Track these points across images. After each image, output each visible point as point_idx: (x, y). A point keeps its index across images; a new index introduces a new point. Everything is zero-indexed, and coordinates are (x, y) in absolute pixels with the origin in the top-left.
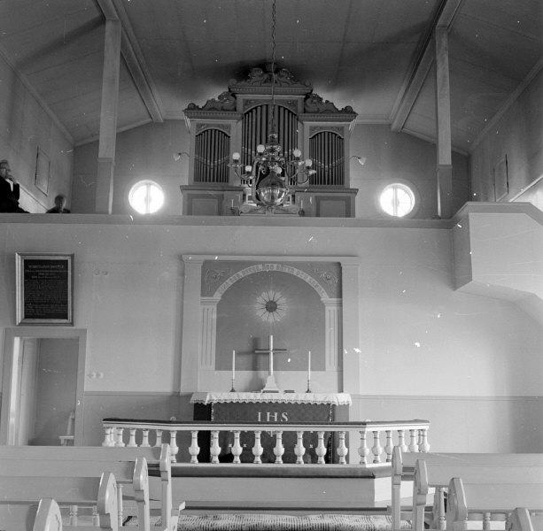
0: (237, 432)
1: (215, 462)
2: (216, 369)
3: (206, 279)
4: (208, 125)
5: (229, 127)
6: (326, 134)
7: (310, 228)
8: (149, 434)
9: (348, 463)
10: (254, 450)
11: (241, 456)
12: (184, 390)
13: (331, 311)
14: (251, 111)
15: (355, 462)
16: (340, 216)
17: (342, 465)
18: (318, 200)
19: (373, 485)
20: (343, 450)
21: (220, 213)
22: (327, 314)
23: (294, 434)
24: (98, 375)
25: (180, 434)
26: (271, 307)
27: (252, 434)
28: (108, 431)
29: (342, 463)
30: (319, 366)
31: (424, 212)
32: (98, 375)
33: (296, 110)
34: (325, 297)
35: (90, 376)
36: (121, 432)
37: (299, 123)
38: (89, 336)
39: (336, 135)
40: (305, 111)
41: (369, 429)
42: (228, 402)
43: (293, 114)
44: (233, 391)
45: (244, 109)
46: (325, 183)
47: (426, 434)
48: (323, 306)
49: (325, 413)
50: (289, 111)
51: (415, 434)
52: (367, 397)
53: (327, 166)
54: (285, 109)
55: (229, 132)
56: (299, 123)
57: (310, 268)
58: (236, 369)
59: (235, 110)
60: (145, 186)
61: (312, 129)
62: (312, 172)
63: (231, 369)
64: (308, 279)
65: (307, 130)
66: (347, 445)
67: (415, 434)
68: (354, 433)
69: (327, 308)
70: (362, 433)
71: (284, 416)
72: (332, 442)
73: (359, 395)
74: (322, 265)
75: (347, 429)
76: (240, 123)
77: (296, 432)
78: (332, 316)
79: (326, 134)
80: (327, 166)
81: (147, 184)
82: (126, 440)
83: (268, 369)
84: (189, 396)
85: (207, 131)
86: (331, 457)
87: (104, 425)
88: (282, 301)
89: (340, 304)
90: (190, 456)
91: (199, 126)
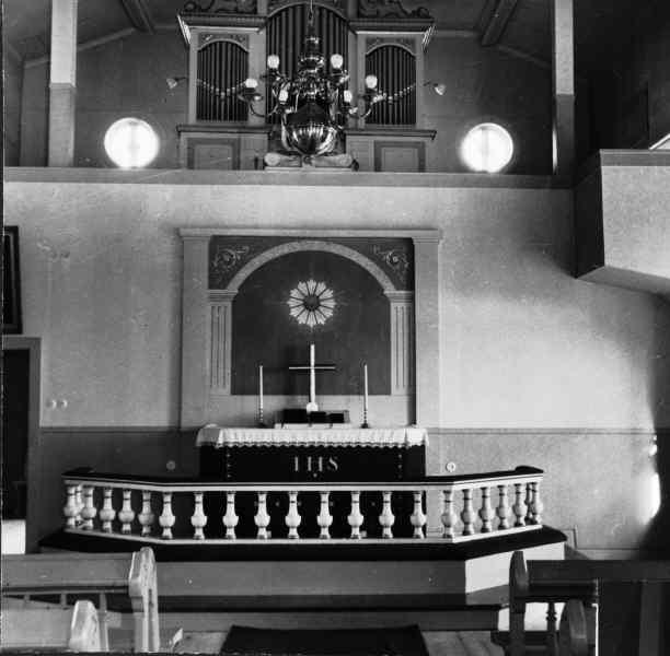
0: (109, 488)
1: (230, 538)
2: (234, 392)
3: (216, 265)
4: (215, 36)
5: (246, 38)
6: (224, 45)
7: (215, 187)
8: (172, 498)
9: (425, 536)
10: (382, 520)
11: (204, 528)
12: (188, 422)
13: (398, 310)
14: (279, 14)
15: (434, 537)
16: (36, 165)
17: (420, 538)
18: (378, 146)
19: (464, 565)
20: (419, 517)
21: (236, 166)
22: (393, 312)
23: (378, 496)
24: (60, 404)
25: (302, 496)
26: (311, 304)
27: (378, 496)
28: (72, 491)
29: (418, 537)
30: (382, 387)
31: (528, 165)
32: (60, 404)
33: (345, 13)
34: (389, 290)
35: (49, 404)
36: (91, 492)
37: (350, 34)
38: (44, 347)
39: (404, 50)
40: (359, 15)
41: (458, 487)
42: (316, 445)
43: (341, 19)
44: (365, 426)
45: (269, 11)
46: (220, 118)
47: (537, 488)
48: (386, 302)
49: (405, 463)
50: (336, 15)
51: (523, 489)
52: (447, 432)
53: (223, 94)
54: (329, 11)
55: (248, 48)
56: (350, 34)
57: (366, 245)
58: (317, 393)
59: (255, 11)
60: (481, 131)
61: (370, 41)
62: (377, 99)
63: (258, 394)
64: (364, 262)
65: (362, 45)
66: (424, 512)
67: (523, 489)
68: (432, 490)
69: (393, 305)
70: (447, 493)
71: (331, 461)
72: (404, 505)
73: (439, 429)
74: (386, 244)
75: (425, 488)
76: (263, 33)
77: (349, 492)
78: (400, 315)
79: (224, 45)
80: (223, 94)
81: (131, 123)
82: (99, 504)
83: (308, 393)
84: (194, 432)
85: (215, 43)
86: (404, 527)
87: (68, 482)
88: (327, 294)
89: (412, 300)
90: (287, 529)
91: (202, 37)
